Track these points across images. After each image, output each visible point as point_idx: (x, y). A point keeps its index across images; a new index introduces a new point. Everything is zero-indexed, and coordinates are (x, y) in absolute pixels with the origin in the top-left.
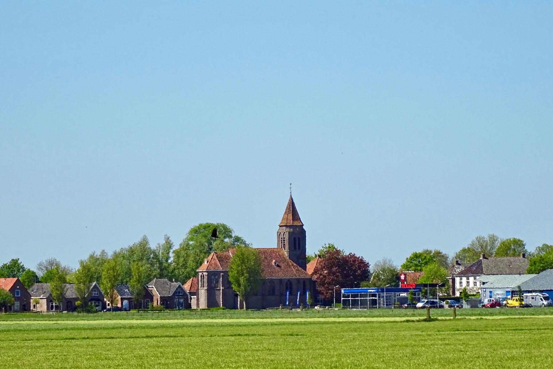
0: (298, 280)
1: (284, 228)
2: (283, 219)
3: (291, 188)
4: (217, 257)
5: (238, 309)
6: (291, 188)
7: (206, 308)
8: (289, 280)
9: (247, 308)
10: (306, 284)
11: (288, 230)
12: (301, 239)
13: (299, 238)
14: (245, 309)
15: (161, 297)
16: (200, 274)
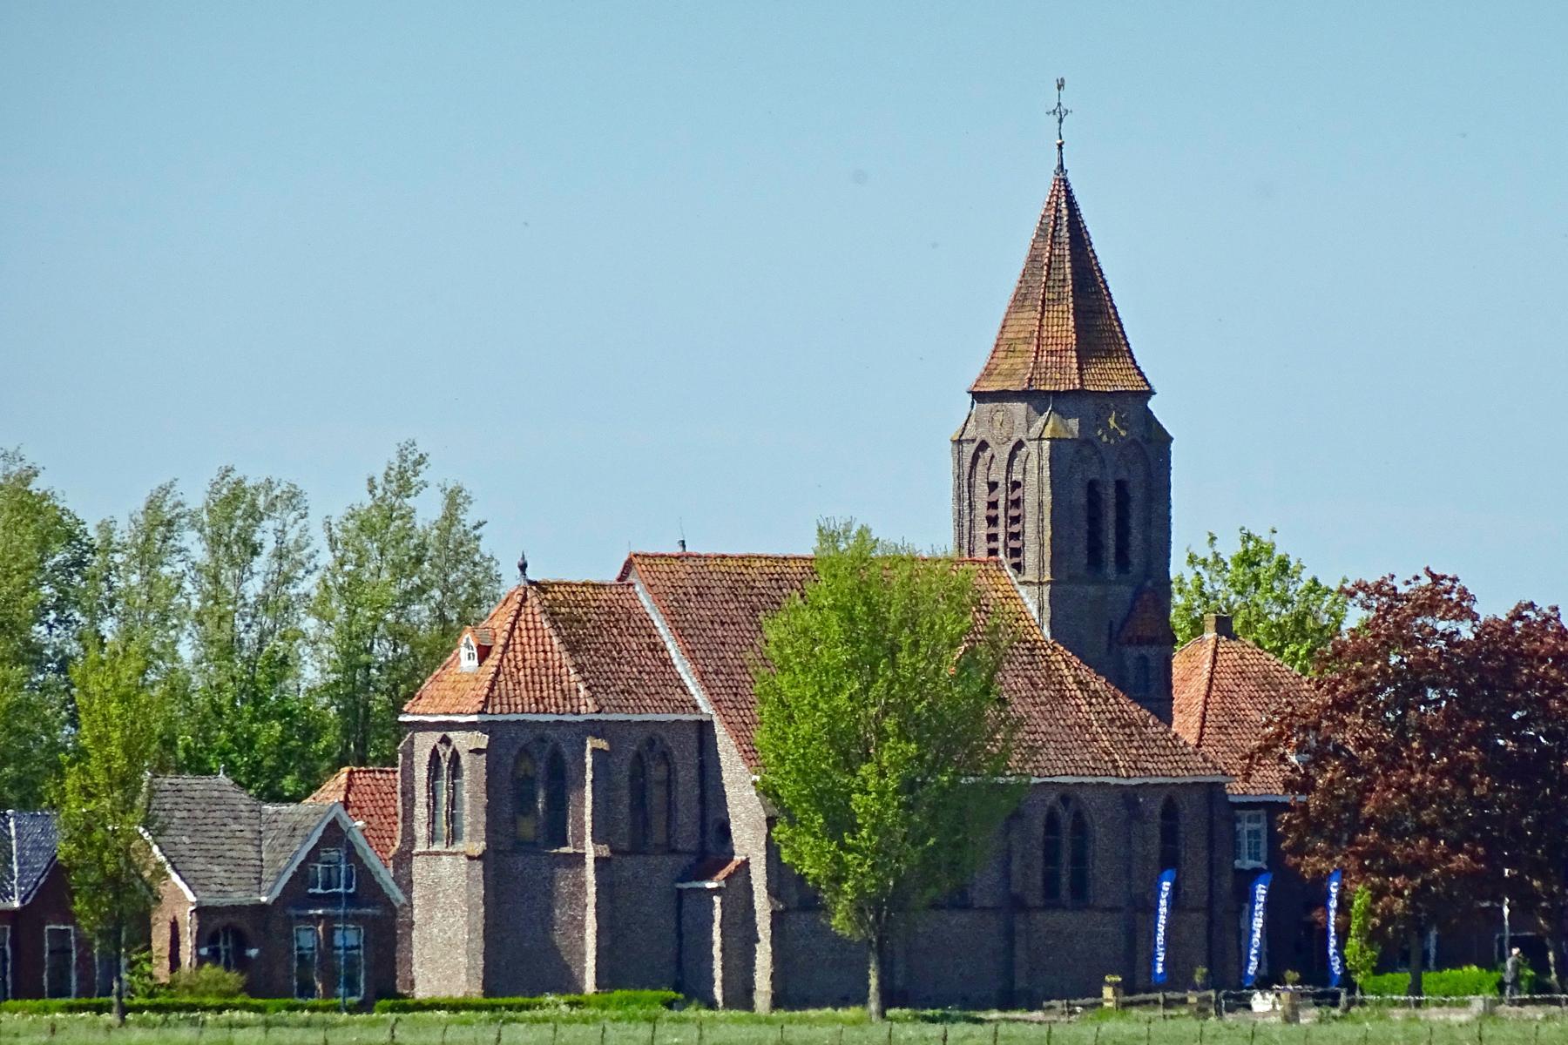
0: (1129, 797)
1: (1020, 408)
2: (1004, 346)
3: (1060, 114)
4: (553, 616)
5: (863, 1001)
6: (1060, 114)
7: (476, 992)
8: (1067, 795)
9: (890, 999)
10: (1189, 822)
11: (1047, 424)
12: (1137, 494)
13: (1121, 486)
14: (873, 1006)
15: (201, 911)
16: (424, 744)
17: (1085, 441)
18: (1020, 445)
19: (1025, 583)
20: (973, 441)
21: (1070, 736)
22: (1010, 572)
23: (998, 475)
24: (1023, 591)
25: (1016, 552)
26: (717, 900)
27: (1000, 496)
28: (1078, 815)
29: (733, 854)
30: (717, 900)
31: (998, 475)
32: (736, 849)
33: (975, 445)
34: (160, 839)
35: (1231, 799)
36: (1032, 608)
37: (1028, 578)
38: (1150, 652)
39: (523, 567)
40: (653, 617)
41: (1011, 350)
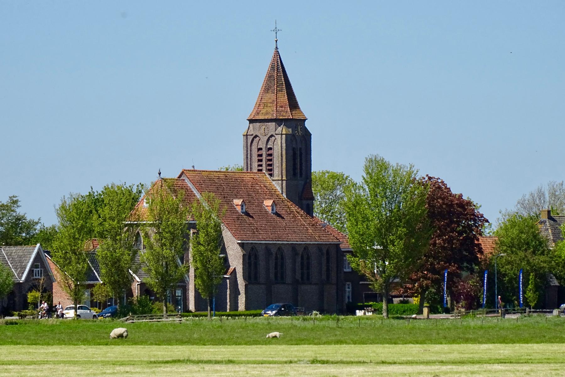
1: (272, 125)
2: (261, 103)
11: (282, 129)
12: (303, 152)
17: (293, 135)
18: (272, 136)
19: (273, 180)
20: (252, 135)
21: (296, 231)
22: (268, 176)
23: (262, 145)
24: (274, 183)
25: (270, 170)
26: (228, 281)
27: (264, 152)
28: (308, 255)
29: (230, 266)
30: (228, 281)
31: (262, 145)
32: (231, 265)
33: (253, 137)
34: (264, 247)
35: (342, 250)
36: (279, 189)
37: (276, 178)
38: (309, 202)
39: (160, 174)
40: (193, 190)
41: (265, 105)
